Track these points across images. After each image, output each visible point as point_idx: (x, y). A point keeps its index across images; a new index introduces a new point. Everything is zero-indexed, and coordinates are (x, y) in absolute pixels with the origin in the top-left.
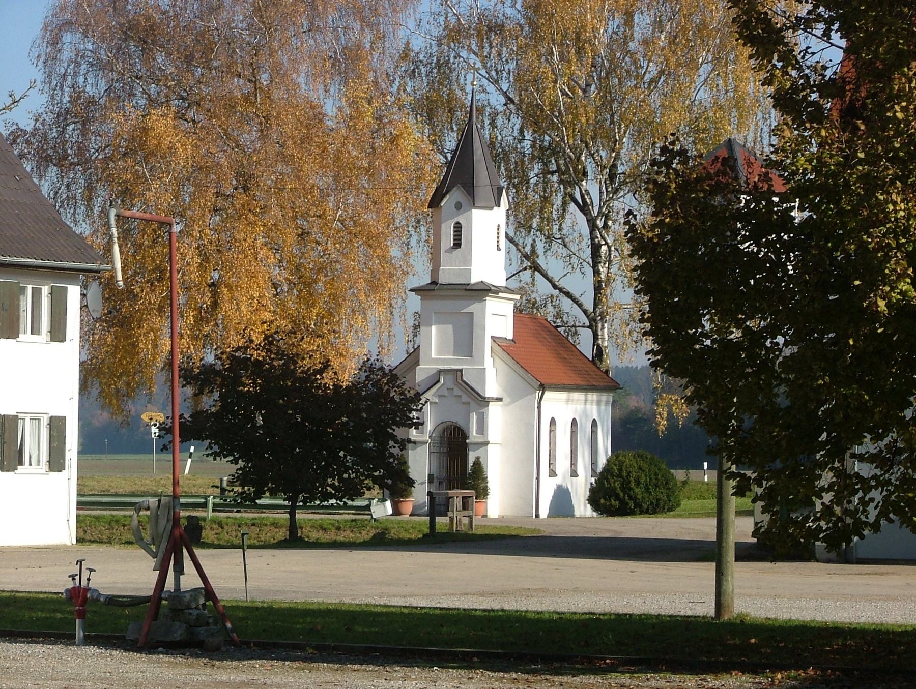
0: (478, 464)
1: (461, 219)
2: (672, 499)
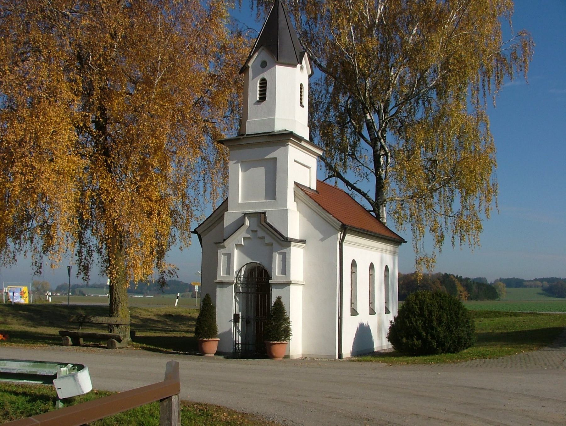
0: (279, 305)
1: (265, 75)
2: (472, 337)
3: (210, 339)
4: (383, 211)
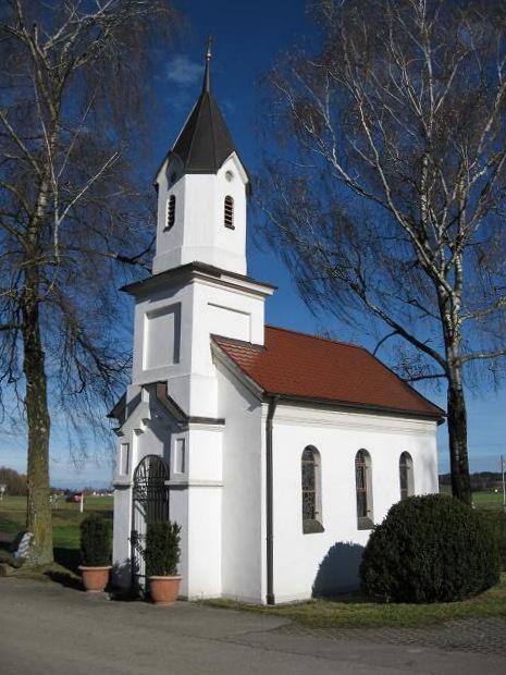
3: (163, 578)
4: (455, 376)
